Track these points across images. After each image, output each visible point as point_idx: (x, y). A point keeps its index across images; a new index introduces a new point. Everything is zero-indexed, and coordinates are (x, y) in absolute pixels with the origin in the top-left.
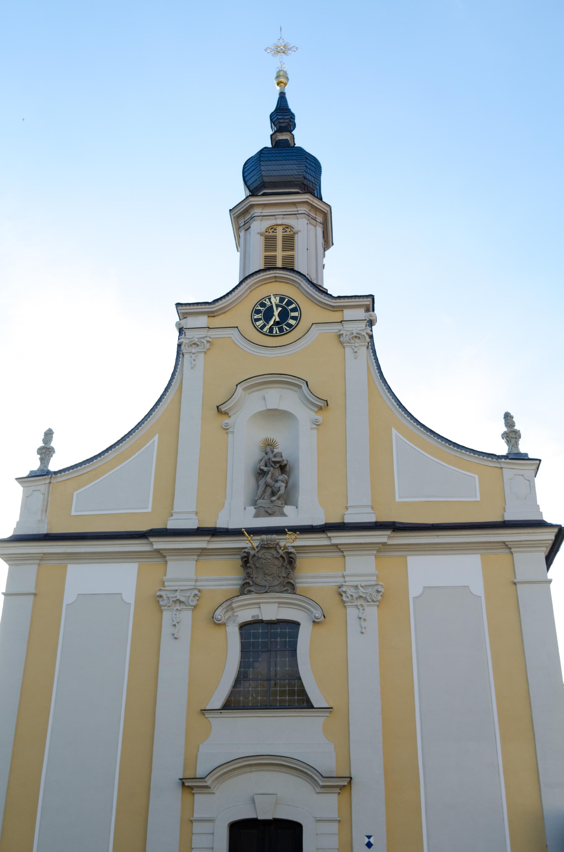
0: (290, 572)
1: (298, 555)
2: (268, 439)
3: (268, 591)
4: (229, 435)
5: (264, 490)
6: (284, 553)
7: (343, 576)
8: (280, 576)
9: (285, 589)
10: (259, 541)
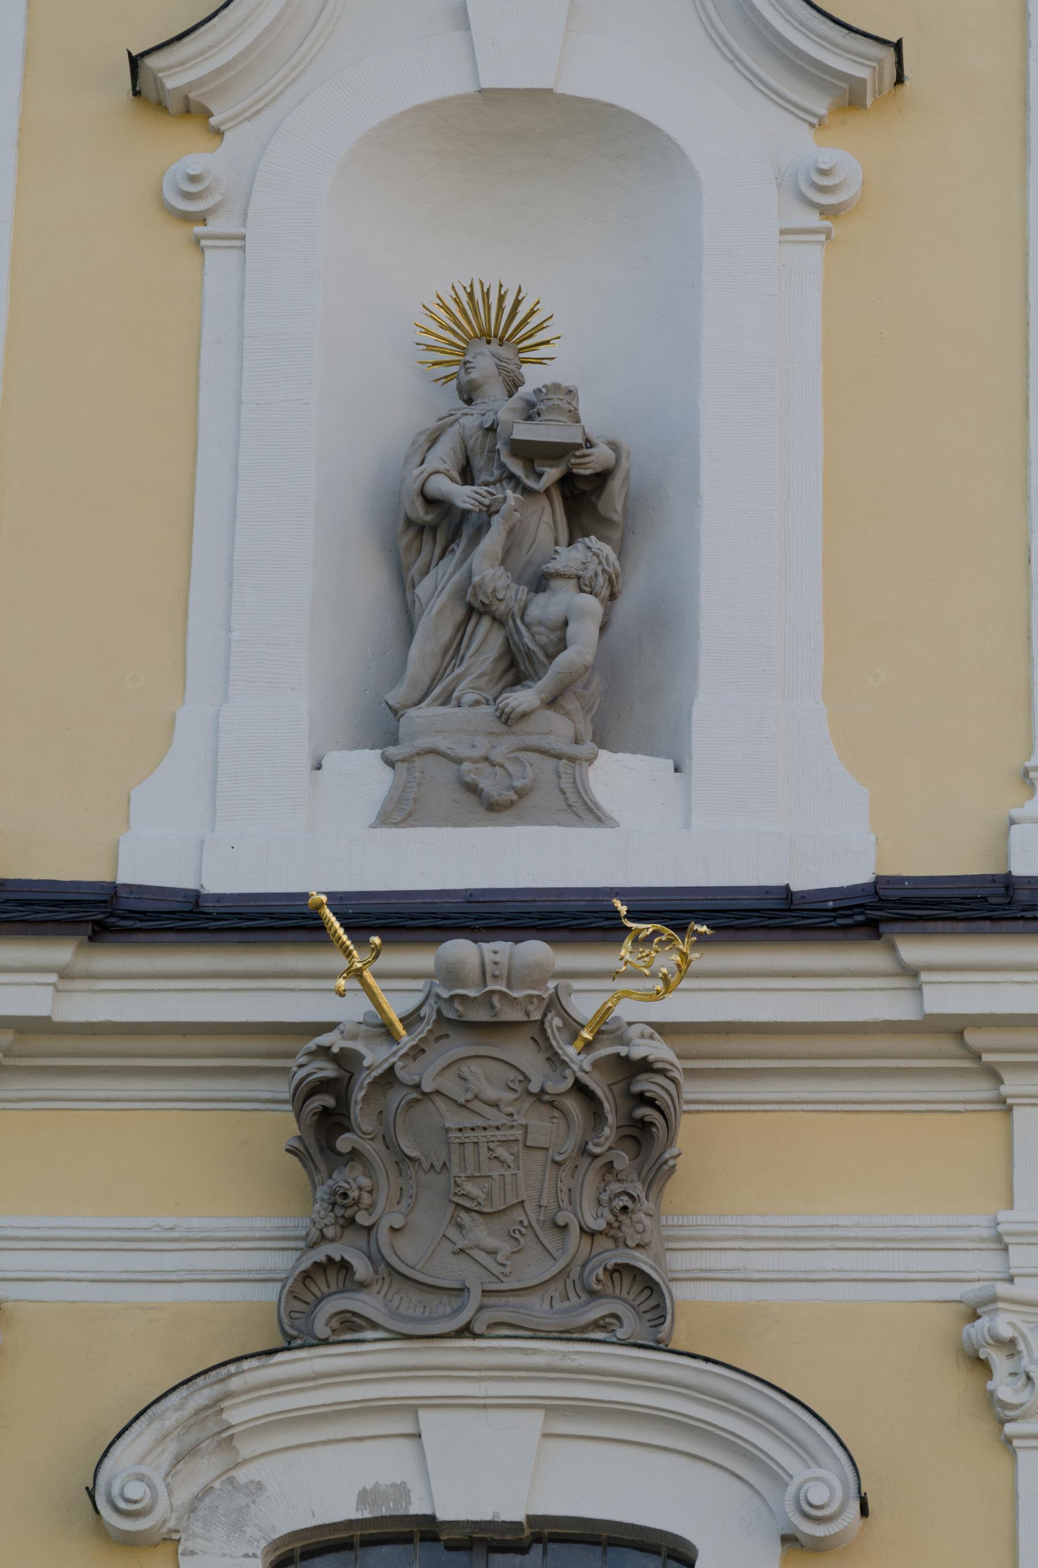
0: (631, 1197)
1: (690, 1090)
2: (486, 295)
3: (479, 1327)
4: (208, 254)
5: (451, 640)
6: (595, 1064)
7: (999, 1238)
8: (561, 1222)
9: (598, 1310)
10: (419, 984)
